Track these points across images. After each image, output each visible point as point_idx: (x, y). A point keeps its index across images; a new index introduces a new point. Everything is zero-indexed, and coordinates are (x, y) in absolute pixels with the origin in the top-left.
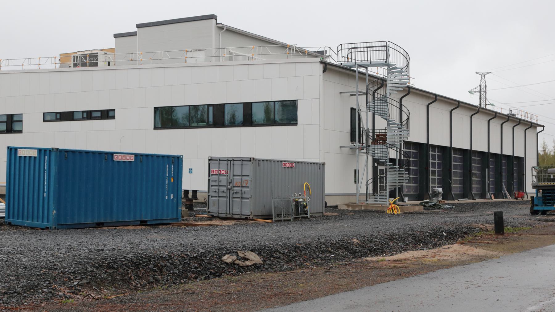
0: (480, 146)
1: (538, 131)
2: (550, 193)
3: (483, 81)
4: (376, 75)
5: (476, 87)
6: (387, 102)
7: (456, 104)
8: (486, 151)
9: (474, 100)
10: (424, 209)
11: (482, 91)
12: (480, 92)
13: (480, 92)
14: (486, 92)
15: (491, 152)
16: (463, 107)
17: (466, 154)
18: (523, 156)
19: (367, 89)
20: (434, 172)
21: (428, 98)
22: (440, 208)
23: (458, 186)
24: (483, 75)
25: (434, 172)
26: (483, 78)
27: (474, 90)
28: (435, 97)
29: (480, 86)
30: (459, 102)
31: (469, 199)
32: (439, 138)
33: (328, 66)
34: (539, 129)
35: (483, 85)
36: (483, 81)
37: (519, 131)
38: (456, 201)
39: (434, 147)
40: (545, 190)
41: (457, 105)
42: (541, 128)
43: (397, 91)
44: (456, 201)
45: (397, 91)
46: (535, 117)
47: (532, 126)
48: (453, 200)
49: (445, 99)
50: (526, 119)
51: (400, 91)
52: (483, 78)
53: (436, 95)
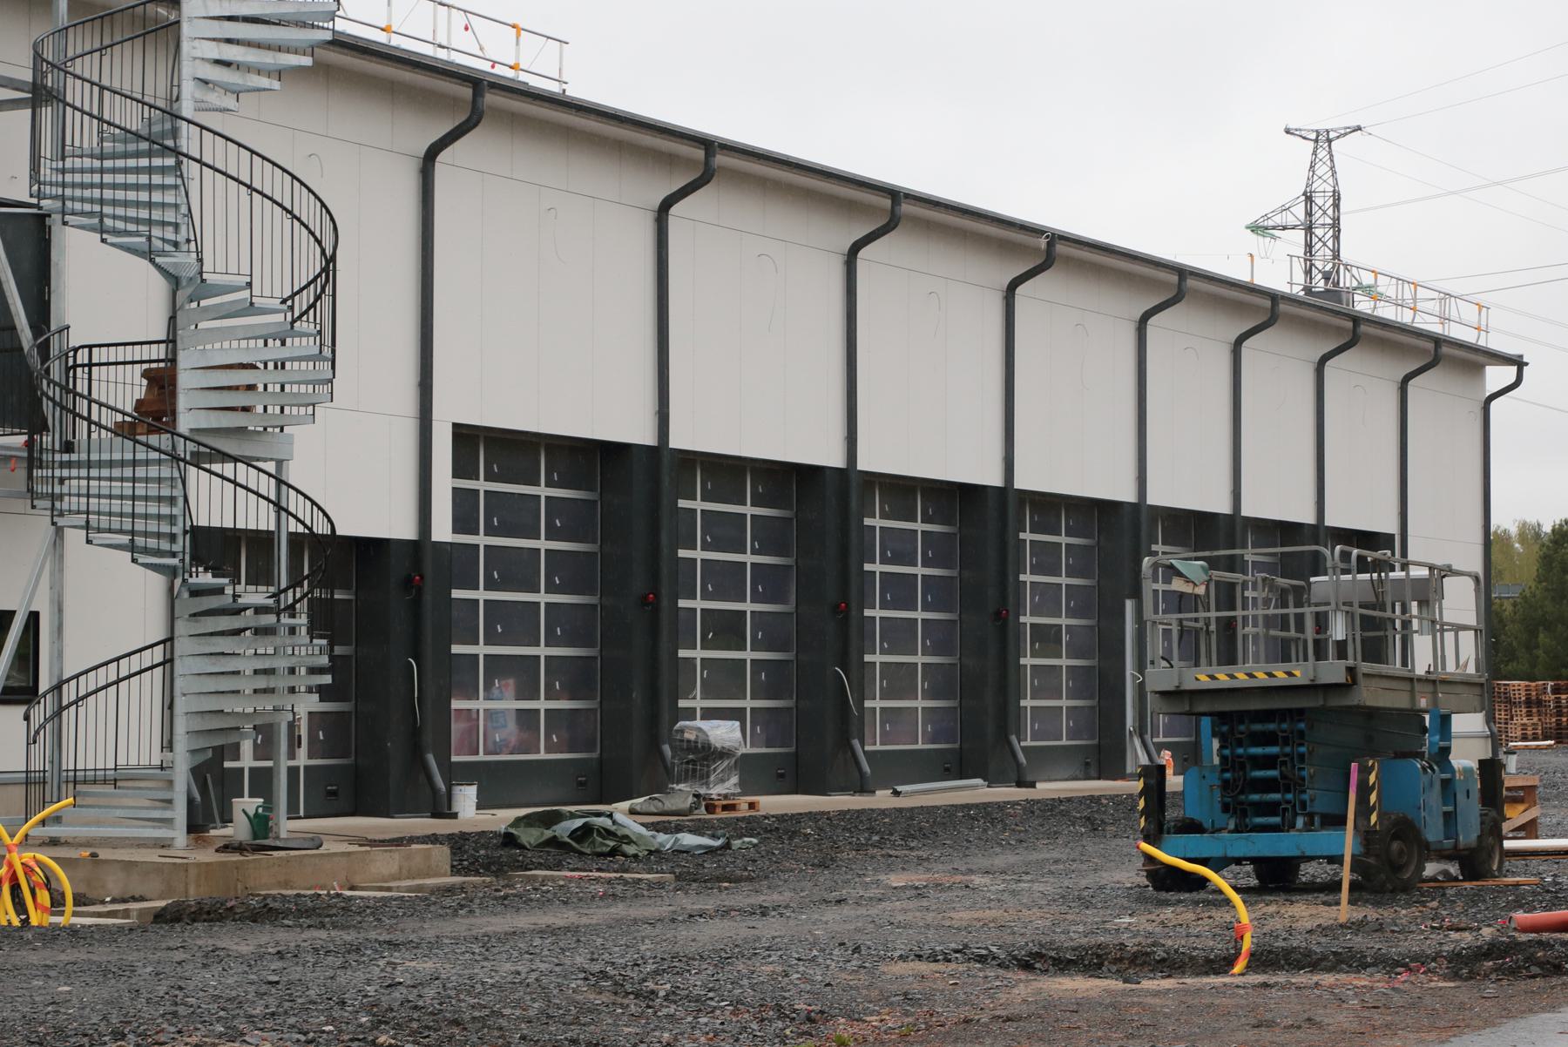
0: (1188, 482)
1: (1492, 386)
2: (1269, 739)
3: (1322, 169)
4: (381, 37)
5: (1285, 199)
6: (176, 152)
7: (689, 162)
8: (1127, 495)
9: (1278, 269)
10: (455, 870)
11: (1319, 217)
12: (1309, 229)
13: (1309, 229)
14: (1336, 225)
15: (1152, 500)
16: (740, 179)
17: (980, 520)
18: (1389, 526)
19: (38, 57)
20: (1047, 639)
21: (849, 208)
22: (614, 852)
23: (1064, 703)
24: (1323, 139)
25: (1047, 639)
26: (1322, 153)
27: (1278, 220)
28: (1175, 278)
29: (1309, 198)
30: (1182, 272)
31: (992, 781)
32: (1074, 457)
33: (490, 98)
34: (1496, 377)
35: (1323, 187)
36: (1322, 169)
37: (1362, 388)
38: (882, 799)
39: (1048, 507)
40: (1241, 716)
41: (1173, 286)
42: (1507, 374)
43: (279, 73)
44: (882, 799)
45: (279, 73)
46: (1469, 313)
47: (1470, 359)
48: (863, 788)
49: (407, 75)
50: (1406, 317)
51: (299, 70)
52: (1322, 153)
53: (895, 195)
